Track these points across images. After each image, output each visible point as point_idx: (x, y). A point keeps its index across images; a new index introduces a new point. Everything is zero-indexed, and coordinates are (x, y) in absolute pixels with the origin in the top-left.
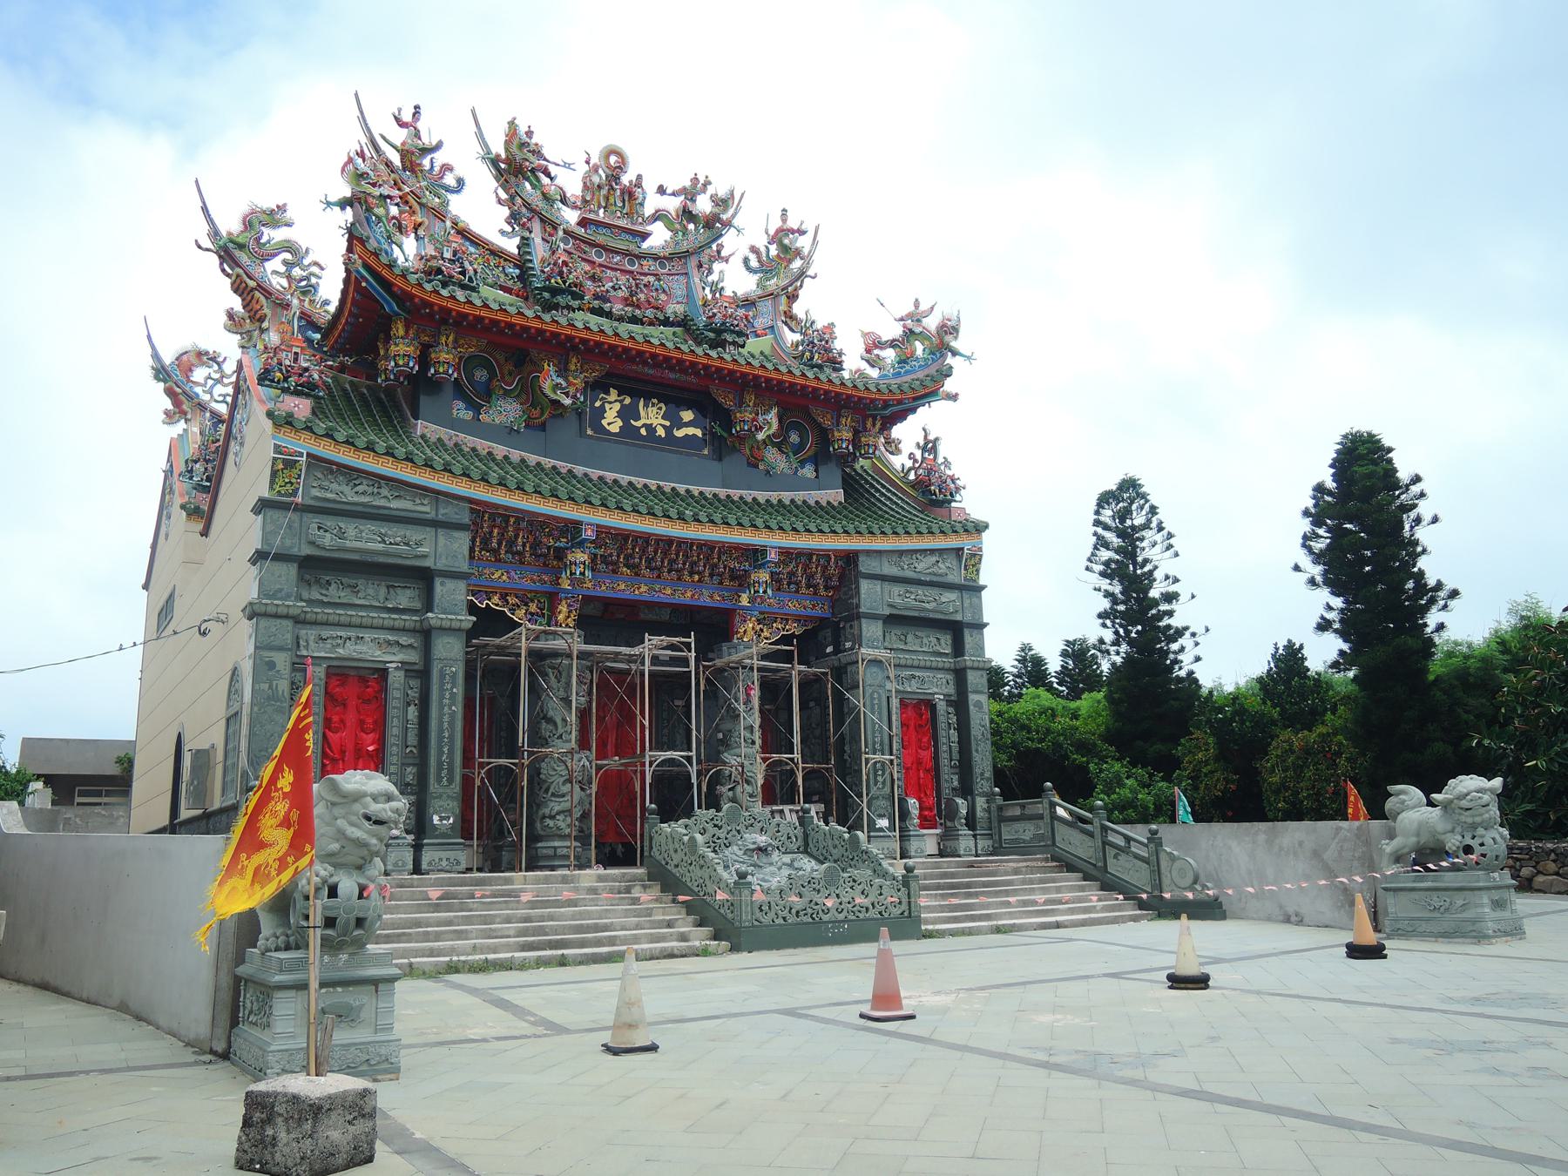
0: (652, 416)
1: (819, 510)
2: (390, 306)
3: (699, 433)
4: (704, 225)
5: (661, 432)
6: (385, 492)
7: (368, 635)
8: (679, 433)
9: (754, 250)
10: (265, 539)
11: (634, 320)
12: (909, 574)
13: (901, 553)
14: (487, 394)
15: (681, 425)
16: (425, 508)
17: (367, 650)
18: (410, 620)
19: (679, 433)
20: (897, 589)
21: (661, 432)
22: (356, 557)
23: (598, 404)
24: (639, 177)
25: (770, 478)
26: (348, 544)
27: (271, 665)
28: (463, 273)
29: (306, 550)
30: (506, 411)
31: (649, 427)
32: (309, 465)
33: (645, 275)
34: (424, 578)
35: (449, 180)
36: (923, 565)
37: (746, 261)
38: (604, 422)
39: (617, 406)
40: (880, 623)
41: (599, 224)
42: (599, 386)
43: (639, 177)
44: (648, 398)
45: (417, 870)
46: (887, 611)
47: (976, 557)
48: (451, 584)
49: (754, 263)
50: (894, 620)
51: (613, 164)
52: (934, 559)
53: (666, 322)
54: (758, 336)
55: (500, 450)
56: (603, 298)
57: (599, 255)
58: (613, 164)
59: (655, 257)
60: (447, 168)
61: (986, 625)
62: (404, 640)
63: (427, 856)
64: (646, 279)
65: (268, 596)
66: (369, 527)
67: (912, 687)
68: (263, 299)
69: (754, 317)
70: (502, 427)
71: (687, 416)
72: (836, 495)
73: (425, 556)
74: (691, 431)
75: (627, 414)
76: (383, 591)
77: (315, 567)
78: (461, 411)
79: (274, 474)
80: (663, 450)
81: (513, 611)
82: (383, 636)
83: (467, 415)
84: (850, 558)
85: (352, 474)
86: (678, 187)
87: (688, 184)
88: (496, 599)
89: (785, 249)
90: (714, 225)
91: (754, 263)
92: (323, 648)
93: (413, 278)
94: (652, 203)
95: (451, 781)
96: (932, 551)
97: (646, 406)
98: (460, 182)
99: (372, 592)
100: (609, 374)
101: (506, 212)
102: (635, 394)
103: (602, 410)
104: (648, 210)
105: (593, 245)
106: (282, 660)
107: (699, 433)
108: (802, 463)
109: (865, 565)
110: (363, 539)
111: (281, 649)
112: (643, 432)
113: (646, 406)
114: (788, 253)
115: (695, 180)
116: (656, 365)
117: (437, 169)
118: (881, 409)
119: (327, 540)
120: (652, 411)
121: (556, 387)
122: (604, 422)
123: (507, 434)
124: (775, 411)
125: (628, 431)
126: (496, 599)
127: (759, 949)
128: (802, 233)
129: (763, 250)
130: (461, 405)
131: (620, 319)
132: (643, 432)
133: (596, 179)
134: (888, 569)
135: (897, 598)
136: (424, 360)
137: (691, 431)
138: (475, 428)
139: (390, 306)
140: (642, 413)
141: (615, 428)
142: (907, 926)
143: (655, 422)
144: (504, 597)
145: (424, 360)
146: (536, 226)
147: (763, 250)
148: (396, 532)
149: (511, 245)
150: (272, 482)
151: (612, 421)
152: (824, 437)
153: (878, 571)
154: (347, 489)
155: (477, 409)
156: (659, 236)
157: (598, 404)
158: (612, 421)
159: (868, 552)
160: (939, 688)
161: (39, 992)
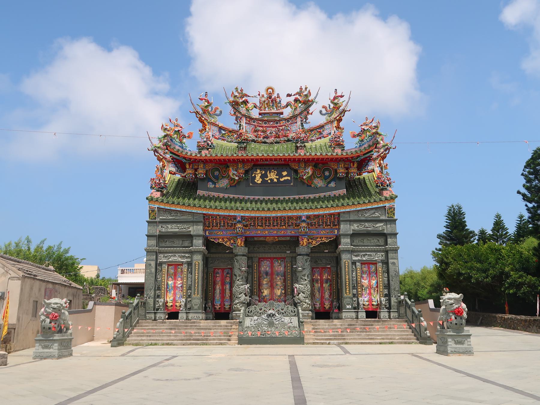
0: (272, 176)
1: (339, 198)
3: (289, 178)
4: (304, 102)
5: (275, 180)
6: (179, 215)
9: (324, 107)
10: (148, 232)
13: (359, 211)
14: (217, 178)
15: (283, 176)
16: (190, 218)
21: (275, 180)
22: (171, 234)
23: (253, 175)
24: (278, 94)
25: (318, 190)
26: (169, 230)
27: (150, 265)
28: (208, 144)
30: (223, 183)
31: (272, 180)
32: (159, 211)
33: (282, 126)
35: (218, 112)
37: (321, 112)
38: (256, 181)
39: (260, 175)
43: (278, 94)
45: (155, 320)
49: (324, 111)
50: (354, 235)
51: (270, 91)
52: (373, 211)
54: (325, 137)
57: (265, 123)
58: (270, 91)
59: (285, 120)
60: (216, 109)
61: (397, 234)
62: (187, 255)
64: (281, 128)
65: (149, 247)
66: (174, 225)
68: (165, 161)
69: (323, 131)
70: (223, 188)
71: (285, 173)
72: (343, 191)
73: (190, 231)
74: (286, 178)
75: (263, 176)
76: (181, 242)
77: (161, 238)
78: (211, 185)
79: (150, 214)
80: (276, 186)
81: (226, 243)
84: (339, 214)
85: (170, 211)
86: (295, 93)
87: (299, 90)
88: (220, 240)
89: (336, 104)
90: (307, 103)
91: (324, 111)
94: (284, 100)
95: (198, 294)
97: (270, 173)
98: (221, 112)
101: (234, 117)
102: (264, 170)
103: (255, 176)
104: (284, 103)
106: (153, 263)
107: (289, 178)
108: (329, 183)
110: (172, 228)
111: (152, 260)
112: (269, 181)
113: (270, 173)
114: (337, 106)
115: (301, 89)
117: (213, 110)
118: (362, 161)
119: (163, 230)
120: (272, 174)
121: (234, 174)
122: (256, 181)
124: (311, 167)
125: (264, 182)
126: (220, 240)
127: (244, 344)
128: (342, 96)
129: (328, 106)
130: (211, 183)
132: (269, 181)
133: (263, 99)
135: (355, 227)
137: (286, 178)
138: (215, 190)
139: (184, 161)
140: (269, 175)
141: (259, 182)
142: (299, 340)
143: (273, 177)
144: (223, 239)
146: (244, 119)
147: (328, 106)
149: (236, 128)
150: (149, 216)
151: (258, 180)
152: (336, 171)
155: (214, 183)
156: (287, 112)
157: (253, 175)
158: (258, 180)
159: (344, 212)
161: (220, 346)
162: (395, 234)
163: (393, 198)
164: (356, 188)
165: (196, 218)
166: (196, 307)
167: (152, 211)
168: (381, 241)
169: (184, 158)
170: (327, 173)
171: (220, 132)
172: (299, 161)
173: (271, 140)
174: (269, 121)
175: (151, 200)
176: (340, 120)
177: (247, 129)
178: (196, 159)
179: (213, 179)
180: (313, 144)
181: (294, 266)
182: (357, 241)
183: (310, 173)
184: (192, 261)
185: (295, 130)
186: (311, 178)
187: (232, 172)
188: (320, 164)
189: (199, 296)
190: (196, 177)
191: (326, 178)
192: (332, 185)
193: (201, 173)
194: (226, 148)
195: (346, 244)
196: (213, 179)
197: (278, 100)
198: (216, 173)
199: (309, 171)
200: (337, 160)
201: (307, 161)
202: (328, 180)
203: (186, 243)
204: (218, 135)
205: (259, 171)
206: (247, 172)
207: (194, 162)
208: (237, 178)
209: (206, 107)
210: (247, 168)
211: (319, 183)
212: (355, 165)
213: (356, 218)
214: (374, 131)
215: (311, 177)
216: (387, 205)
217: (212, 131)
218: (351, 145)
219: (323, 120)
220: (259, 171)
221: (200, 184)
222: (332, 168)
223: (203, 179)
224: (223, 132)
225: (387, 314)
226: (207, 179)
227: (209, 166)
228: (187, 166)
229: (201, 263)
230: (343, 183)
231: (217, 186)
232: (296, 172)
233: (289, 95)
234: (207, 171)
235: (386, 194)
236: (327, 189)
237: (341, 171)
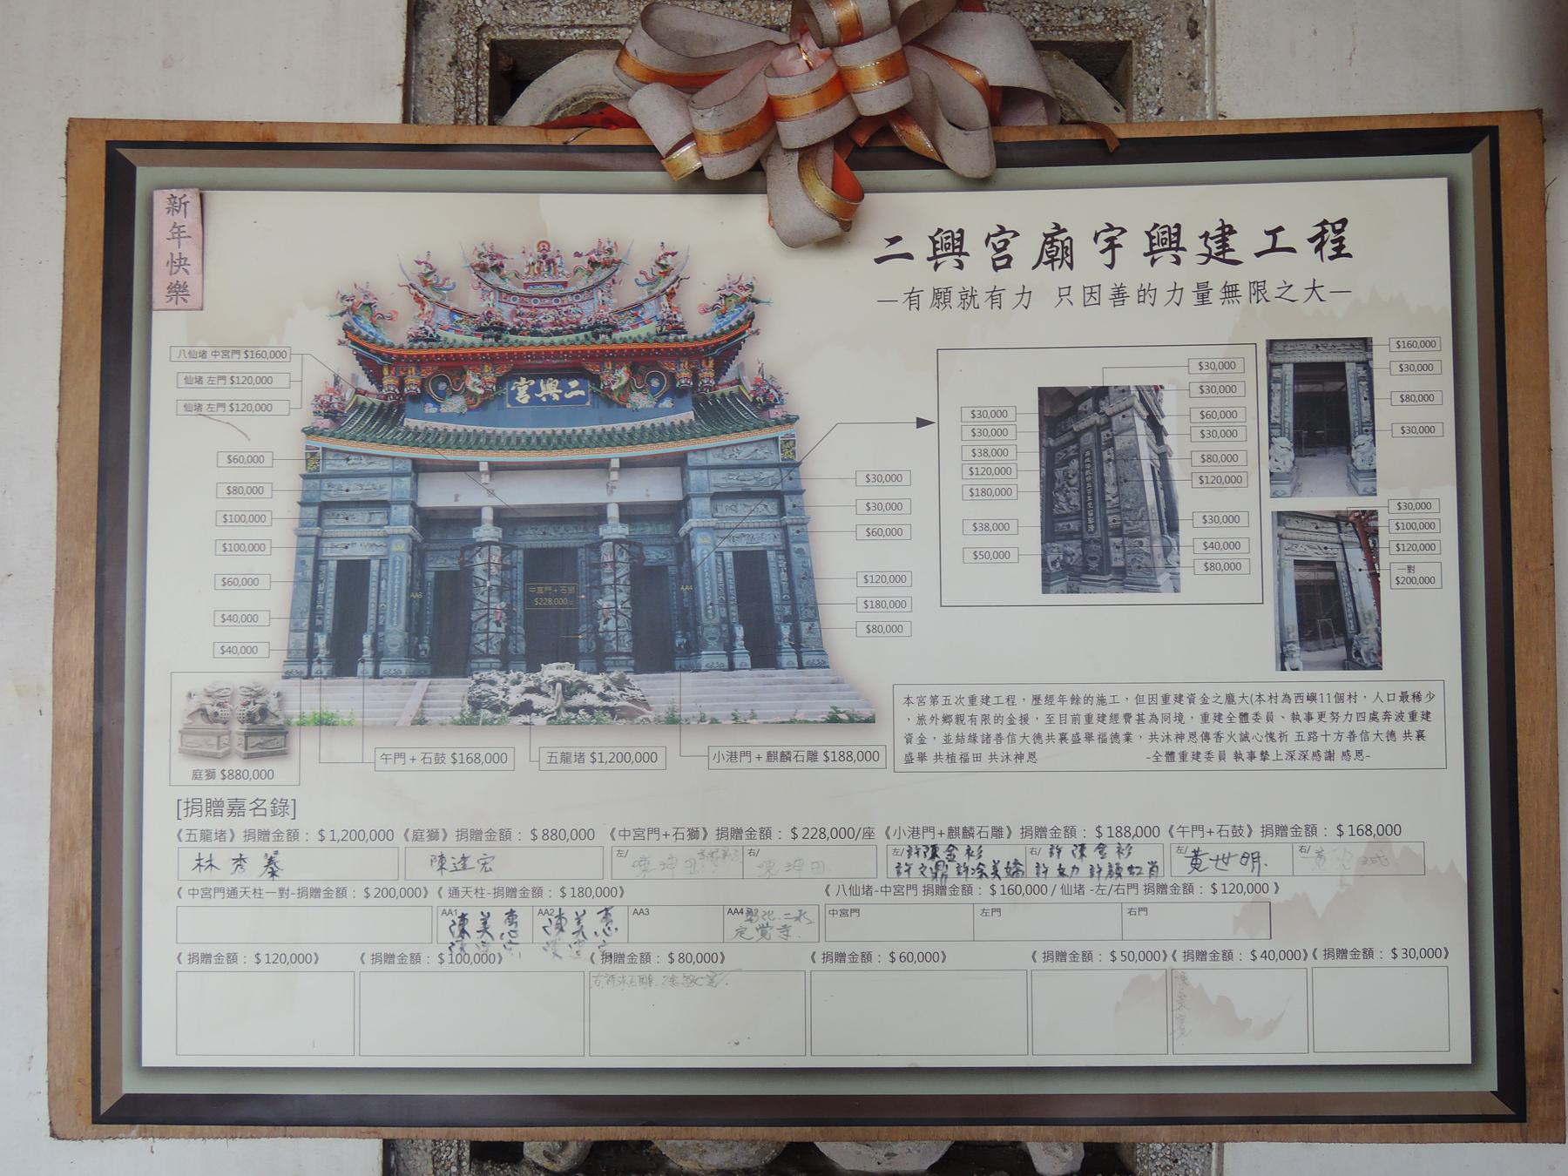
0: (550, 388)
2: (379, 361)
3: (582, 393)
5: (556, 398)
7: (359, 541)
8: (568, 396)
11: (557, 333)
12: (732, 462)
13: (724, 447)
15: (569, 390)
16: (386, 466)
17: (358, 551)
18: (1335, 539)
19: (568, 396)
20: (723, 474)
21: (556, 398)
25: (636, 413)
27: (303, 562)
29: (324, 499)
30: (455, 404)
31: (548, 396)
34: (385, 504)
36: (744, 454)
40: (708, 500)
41: (534, 285)
42: (512, 376)
44: (545, 378)
46: (714, 490)
47: (790, 442)
48: (400, 508)
50: (716, 497)
52: (752, 448)
53: (578, 330)
55: (451, 427)
56: (538, 325)
63: (383, 668)
67: (742, 544)
71: (574, 384)
72: (688, 416)
74: (577, 393)
75: (533, 391)
82: (371, 541)
83: (434, 410)
84: (685, 453)
85: (347, 455)
89: (663, 266)
91: (642, 280)
92: (334, 552)
93: (407, 345)
96: (751, 443)
99: (360, 517)
100: (513, 370)
102: (536, 378)
105: (531, 297)
106: (309, 559)
107: (582, 393)
108: (660, 400)
109: (693, 459)
114: (665, 270)
116: (539, 358)
118: (724, 349)
120: (550, 385)
123: (458, 417)
125: (534, 401)
131: (548, 335)
134: (713, 460)
135: (721, 480)
136: (402, 385)
137: (577, 393)
138: (439, 417)
139: (379, 361)
141: (525, 401)
145: (402, 385)
148: (366, 483)
151: (523, 397)
152: (673, 378)
153: (704, 463)
154: (344, 463)
155: (438, 405)
158: (523, 397)
160: (766, 539)
162: (800, 492)
163: (790, 420)
164: (716, 413)
165: (399, 466)
166: (394, 650)
167: (311, 455)
168: (772, 507)
169: (379, 354)
170: (655, 383)
171: (453, 320)
172: (600, 357)
173: (546, 330)
174: (541, 297)
175: (310, 432)
176: (671, 295)
177: (504, 313)
178: (401, 356)
179: (435, 396)
180: (625, 335)
181: (417, 596)
182: (724, 507)
183: (625, 379)
184: (388, 554)
185: (588, 311)
186: (627, 388)
187: (472, 381)
188: (642, 361)
189: (402, 626)
190: (402, 393)
191: (654, 391)
192: (667, 403)
193: (413, 381)
194: (464, 339)
195: (702, 515)
196: (435, 396)
197: (558, 261)
198: (442, 386)
199: (623, 375)
200: (677, 354)
201: (618, 357)
202: (659, 395)
203: (378, 519)
204: (447, 322)
205: (523, 380)
206: (500, 382)
207: (399, 361)
208: (480, 391)
209: (428, 275)
210: (499, 374)
211: (640, 400)
212: (711, 363)
213: (719, 461)
214: (745, 294)
215: (624, 386)
216: (780, 433)
217: (442, 316)
218: (699, 325)
219: (638, 295)
220: (523, 380)
221: (409, 407)
222: (666, 372)
223: (415, 398)
224: (457, 318)
225: (794, 659)
226: (420, 398)
227: (427, 372)
228: (386, 372)
229: (407, 558)
230: (688, 400)
231: (443, 410)
232: (596, 380)
233: (577, 255)
234: (423, 380)
235: (774, 413)
236: (656, 412)
237: (684, 376)
